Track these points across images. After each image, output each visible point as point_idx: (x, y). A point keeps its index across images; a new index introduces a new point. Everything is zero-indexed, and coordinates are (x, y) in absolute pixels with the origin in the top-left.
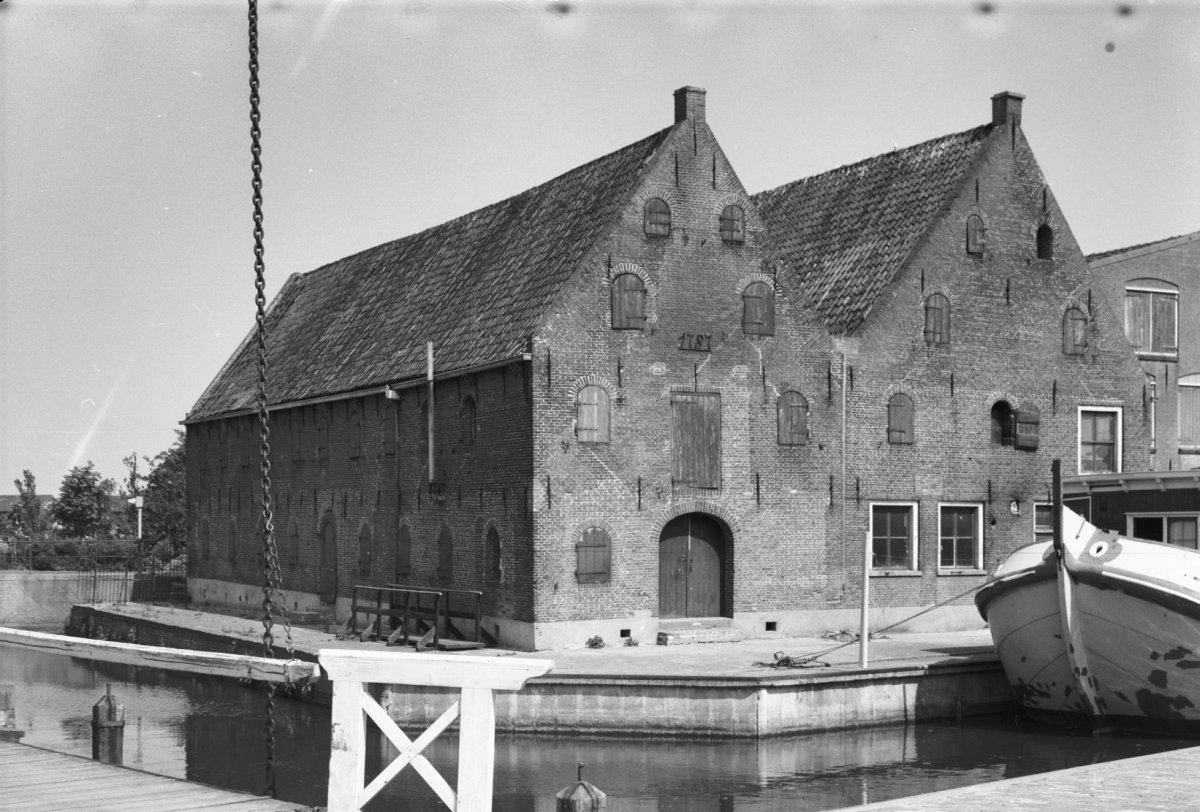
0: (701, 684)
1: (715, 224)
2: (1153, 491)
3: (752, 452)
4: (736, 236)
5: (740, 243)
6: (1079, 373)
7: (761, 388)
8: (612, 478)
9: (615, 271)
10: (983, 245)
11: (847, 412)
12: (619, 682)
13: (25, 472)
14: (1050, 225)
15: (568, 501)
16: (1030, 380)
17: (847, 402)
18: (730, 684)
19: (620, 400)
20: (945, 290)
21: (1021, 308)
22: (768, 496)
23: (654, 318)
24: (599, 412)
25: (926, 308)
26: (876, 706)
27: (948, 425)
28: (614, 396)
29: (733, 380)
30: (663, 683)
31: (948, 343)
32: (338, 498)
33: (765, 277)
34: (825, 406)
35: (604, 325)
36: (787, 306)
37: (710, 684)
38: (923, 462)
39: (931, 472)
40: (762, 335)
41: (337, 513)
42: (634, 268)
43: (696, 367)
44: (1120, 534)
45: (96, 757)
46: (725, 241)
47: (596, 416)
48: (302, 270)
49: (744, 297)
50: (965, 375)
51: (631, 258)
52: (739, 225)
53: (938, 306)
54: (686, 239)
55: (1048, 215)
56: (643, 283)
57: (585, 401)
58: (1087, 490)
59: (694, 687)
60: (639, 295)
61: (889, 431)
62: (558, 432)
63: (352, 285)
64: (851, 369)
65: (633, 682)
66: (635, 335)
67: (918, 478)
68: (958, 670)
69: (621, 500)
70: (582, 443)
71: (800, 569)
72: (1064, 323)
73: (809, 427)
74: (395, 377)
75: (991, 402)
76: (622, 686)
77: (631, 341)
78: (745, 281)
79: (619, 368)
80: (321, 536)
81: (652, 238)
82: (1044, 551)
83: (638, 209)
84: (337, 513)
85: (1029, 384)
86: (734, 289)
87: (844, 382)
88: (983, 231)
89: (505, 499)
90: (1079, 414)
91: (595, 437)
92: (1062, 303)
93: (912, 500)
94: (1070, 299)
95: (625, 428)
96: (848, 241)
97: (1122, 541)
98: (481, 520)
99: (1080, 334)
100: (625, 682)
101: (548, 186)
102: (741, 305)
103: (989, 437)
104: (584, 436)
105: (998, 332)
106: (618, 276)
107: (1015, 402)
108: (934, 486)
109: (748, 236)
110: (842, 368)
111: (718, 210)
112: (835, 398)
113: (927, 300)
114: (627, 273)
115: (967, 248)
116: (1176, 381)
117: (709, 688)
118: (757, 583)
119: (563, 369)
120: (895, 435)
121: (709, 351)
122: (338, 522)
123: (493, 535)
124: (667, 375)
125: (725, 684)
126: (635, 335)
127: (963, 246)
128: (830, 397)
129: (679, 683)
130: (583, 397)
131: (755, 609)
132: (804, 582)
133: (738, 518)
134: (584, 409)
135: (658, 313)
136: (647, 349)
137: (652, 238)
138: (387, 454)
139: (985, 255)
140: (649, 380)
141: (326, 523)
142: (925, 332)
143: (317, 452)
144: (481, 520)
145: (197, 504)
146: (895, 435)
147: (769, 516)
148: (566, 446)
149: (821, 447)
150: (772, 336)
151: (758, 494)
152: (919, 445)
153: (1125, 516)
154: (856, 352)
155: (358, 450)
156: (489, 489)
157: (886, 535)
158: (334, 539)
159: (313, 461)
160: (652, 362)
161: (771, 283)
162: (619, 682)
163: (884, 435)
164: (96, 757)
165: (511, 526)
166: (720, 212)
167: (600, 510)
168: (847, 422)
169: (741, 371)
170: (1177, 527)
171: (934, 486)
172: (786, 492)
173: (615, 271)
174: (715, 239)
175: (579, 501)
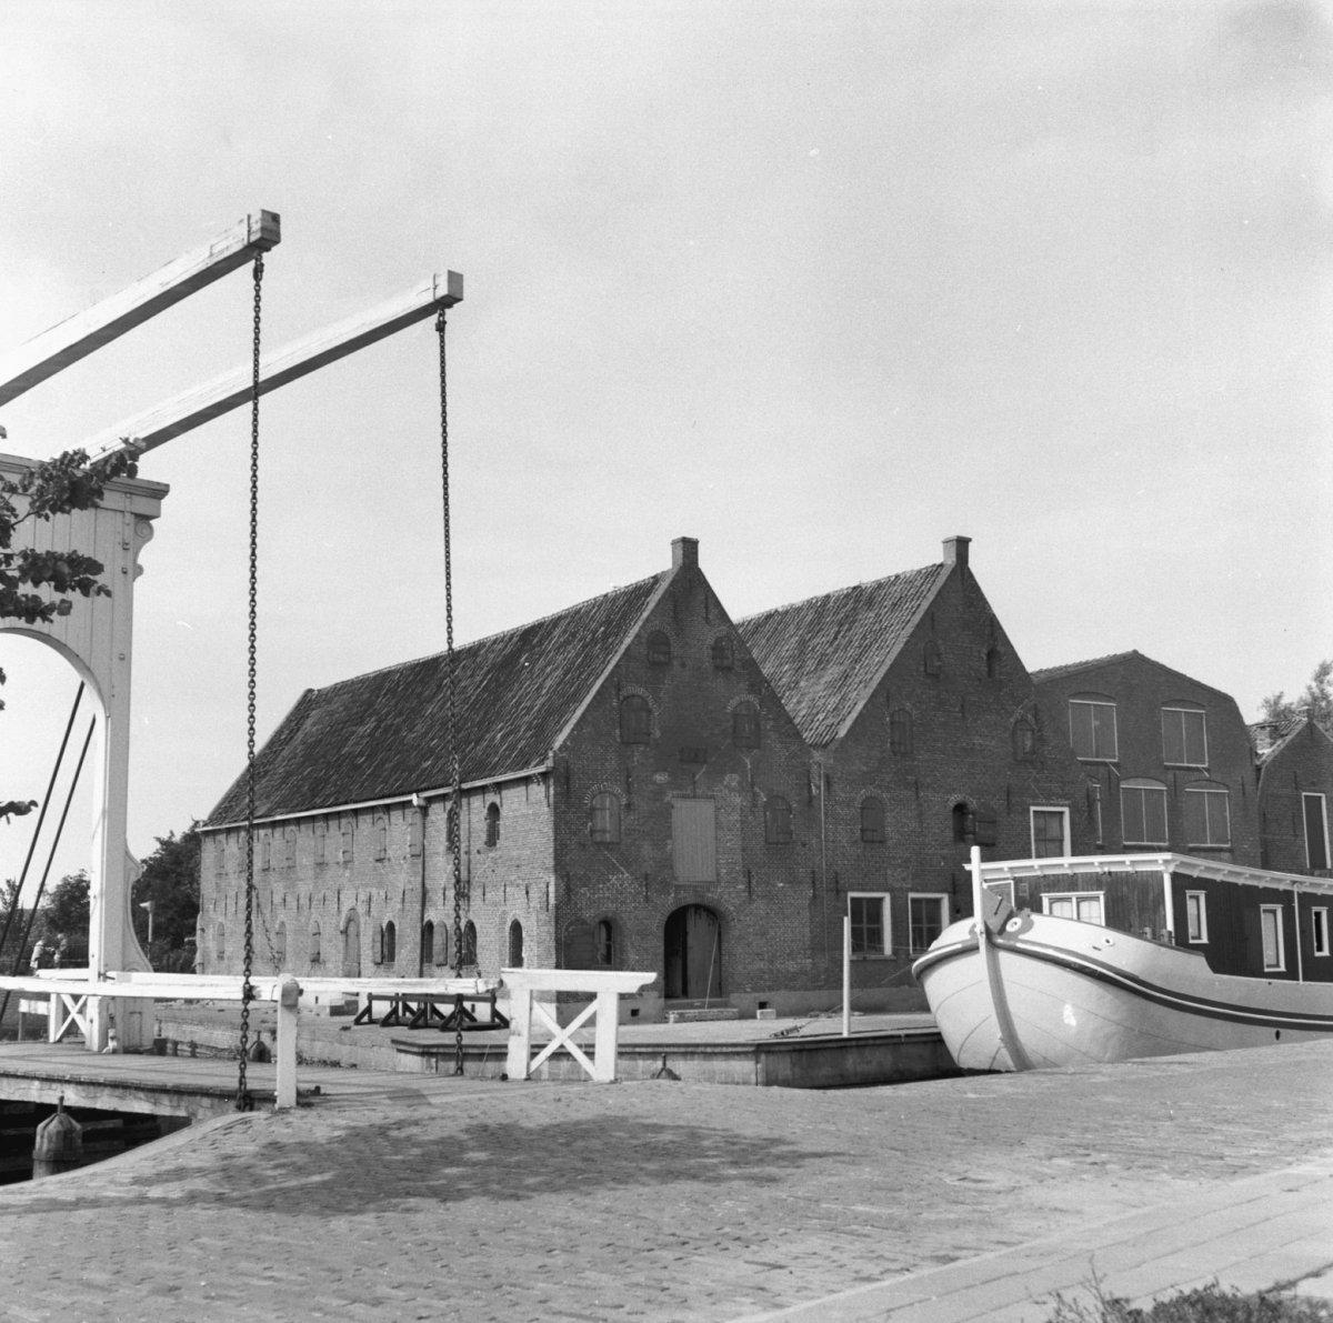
0: (709, 1050)
1: (708, 652)
2: (1273, 889)
3: (743, 850)
4: (726, 663)
5: (729, 669)
6: (1029, 778)
7: (750, 794)
8: (622, 873)
9: (624, 693)
10: (940, 667)
11: (826, 814)
12: (638, 1050)
13: (8, 882)
14: (998, 648)
15: (585, 894)
16: (985, 784)
17: (825, 805)
18: (734, 1050)
19: (628, 806)
20: (908, 706)
21: (975, 720)
22: (758, 890)
23: (658, 734)
24: (611, 815)
25: (892, 723)
26: (859, 1069)
27: (914, 825)
28: (624, 801)
29: (726, 786)
30: (676, 1050)
31: (912, 753)
32: (362, 897)
33: (751, 698)
34: (806, 809)
35: (615, 740)
36: (771, 723)
37: (717, 1050)
38: (894, 858)
39: (900, 866)
40: (750, 748)
41: (361, 909)
42: (641, 691)
43: (694, 776)
44: (1033, 910)
45: (620, 1046)
46: (717, 667)
47: (608, 819)
48: (316, 687)
49: (735, 715)
50: (928, 780)
51: (637, 683)
52: (729, 653)
53: (902, 720)
54: (683, 665)
55: (996, 640)
56: (647, 704)
57: (598, 806)
58: (1009, 875)
59: (702, 1053)
60: (644, 714)
61: (862, 830)
62: (575, 834)
63: (370, 704)
64: (827, 777)
65: (650, 1050)
66: (642, 749)
67: (889, 872)
68: (930, 1038)
69: (630, 893)
70: (597, 843)
71: (788, 955)
72: (1014, 733)
73: (792, 827)
74: (423, 786)
75: (952, 805)
76: (640, 1053)
77: (637, 755)
78: (734, 702)
79: (628, 777)
80: (345, 932)
81: (655, 665)
82: (1030, 932)
83: (643, 640)
84: (361, 909)
85: (985, 788)
86: (725, 708)
87: (822, 788)
88: (939, 655)
89: (527, 893)
90: (1032, 814)
91: (608, 837)
92: (1011, 716)
93: (885, 891)
94: (1019, 712)
95: (634, 830)
96: (823, 662)
97: (1035, 917)
98: (504, 912)
99: (1029, 743)
100: (643, 1050)
101: (556, 621)
102: (731, 723)
103: (952, 835)
104: (598, 838)
105: (955, 743)
106: (626, 698)
107: (973, 804)
108: (904, 879)
109: (736, 662)
110: (820, 776)
111: (710, 641)
112: (815, 802)
113: (892, 716)
114: (633, 696)
115: (925, 671)
116: (1118, 785)
117: (715, 1054)
118: (750, 967)
119: (579, 779)
120: (869, 835)
121: (705, 762)
122: (362, 920)
123: (516, 928)
124: (668, 783)
125: (730, 1049)
126: (642, 749)
127: (922, 669)
128: (810, 802)
129: (690, 1049)
130: (597, 803)
131: (748, 990)
132: (792, 966)
133: (732, 908)
134: (598, 813)
135: (660, 729)
136: (651, 760)
137: (655, 665)
138: (412, 856)
139: (942, 676)
140: (651, 787)
141: (349, 920)
142: (891, 744)
143: (341, 854)
144: (504, 912)
145: (211, 907)
146: (869, 835)
147: (760, 906)
148: (583, 846)
149: (804, 845)
150: (759, 748)
151: (750, 887)
152: (890, 843)
153: (1041, 898)
154: (832, 761)
155: (383, 853)
156: (512, 884)
157: (868, 923)
158: (358, 935)
159: (338, 863)
160: (656, 771)
161: (756, 703)
162: (638, 1050)
163: (858, 833)
164: (620, 1046)
165: (534, 918)
166: (712, 643)
167: (612, 902)
168: (826, 823)
169: (732, 780)
170: (1056, 906)
171: (904, 879)
172: (774, 886)
173: (624, 693)
174: (708, 664)
175: (594, 894)
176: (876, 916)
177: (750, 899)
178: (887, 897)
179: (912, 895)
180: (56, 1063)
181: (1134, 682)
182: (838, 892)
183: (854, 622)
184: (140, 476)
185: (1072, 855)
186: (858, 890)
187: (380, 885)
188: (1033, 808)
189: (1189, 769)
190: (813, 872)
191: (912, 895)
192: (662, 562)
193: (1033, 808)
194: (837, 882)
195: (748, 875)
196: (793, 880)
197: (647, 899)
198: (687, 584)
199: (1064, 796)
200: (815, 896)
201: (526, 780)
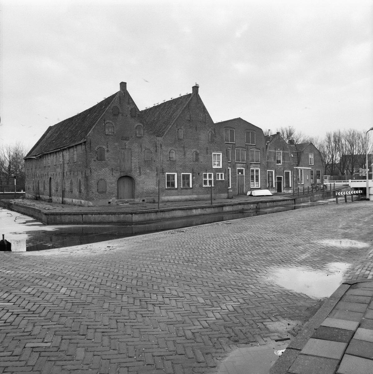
9: (106, 122)
22: (142, 172)
79: (107, 144)
147: (143, 177)
149: (154, 161)
176: (188, 178)
177: (140, 175)
178: (176, 174)
179: (182, 173)
180: (276, 206)
181: (238, 125)
182: (163, 173)
183: (171, 108)
184: (191, 93)
185: (366, 169)
186: (168, 172)
187: (55, 171)
188: (213, 153)
189: (251, 145)
190: (157, 168)
191: (182, 173)
192: (117, 89)
193: (213, 153)
194: (163, 170)
195: (140, 168)
196: (152, 170)
197: (112, 175)
198: (123, 97)
199: (221, 150)
200: (157, 174)
201: (81, 144)
